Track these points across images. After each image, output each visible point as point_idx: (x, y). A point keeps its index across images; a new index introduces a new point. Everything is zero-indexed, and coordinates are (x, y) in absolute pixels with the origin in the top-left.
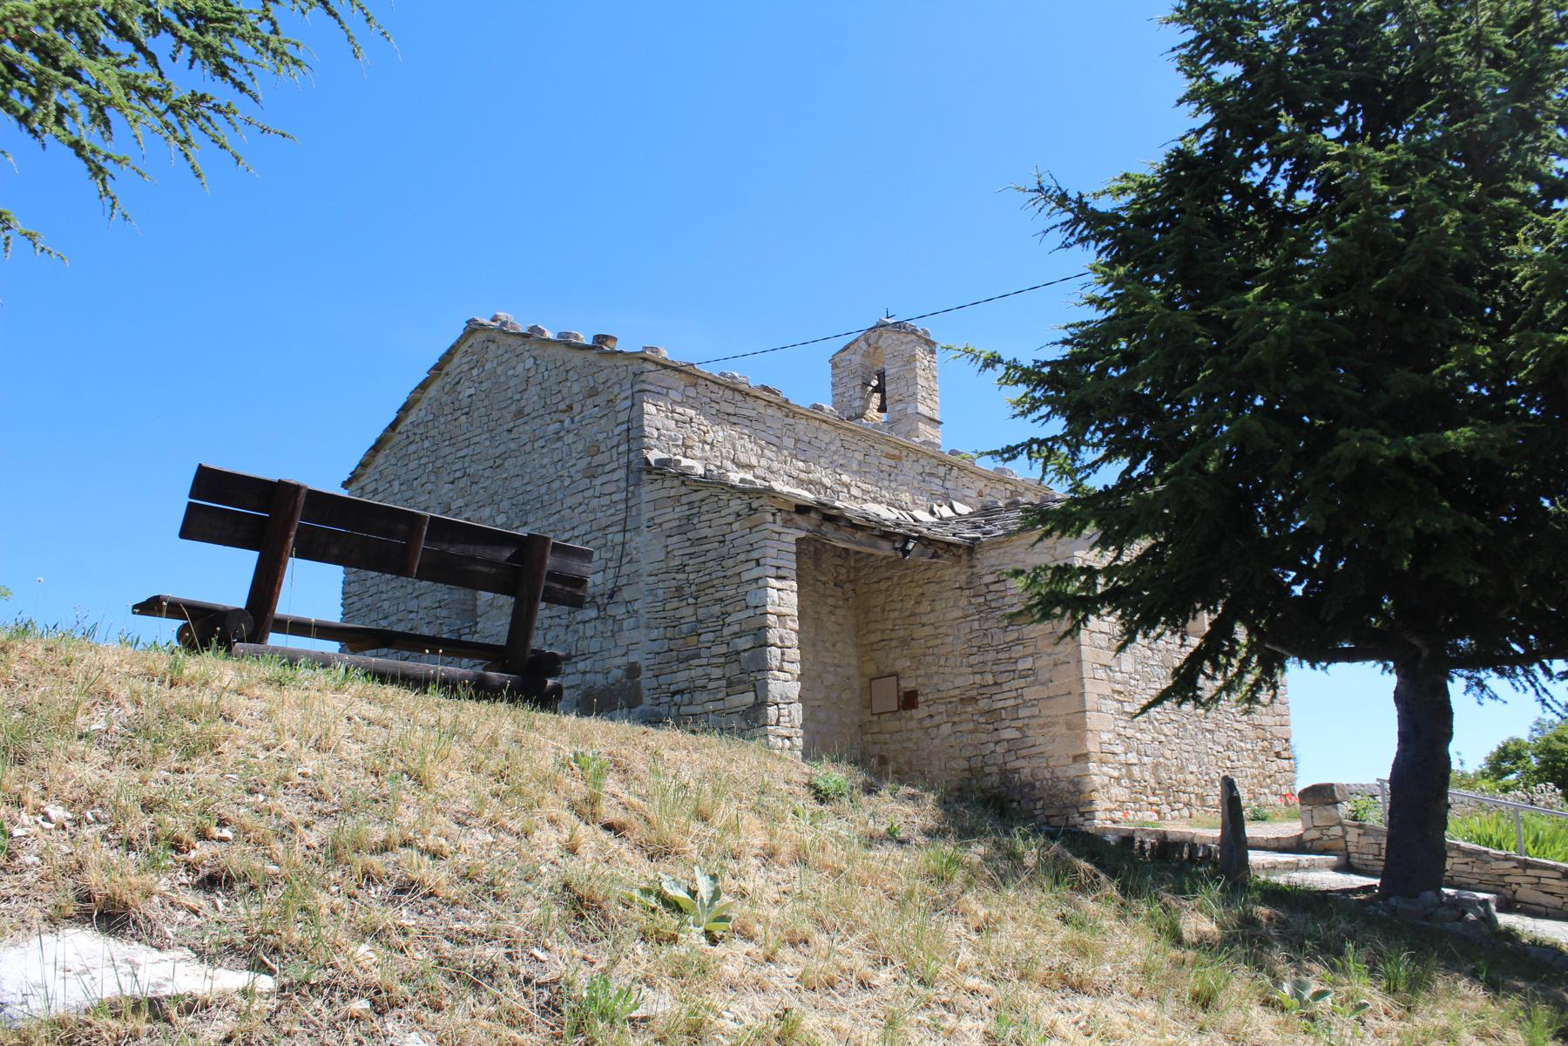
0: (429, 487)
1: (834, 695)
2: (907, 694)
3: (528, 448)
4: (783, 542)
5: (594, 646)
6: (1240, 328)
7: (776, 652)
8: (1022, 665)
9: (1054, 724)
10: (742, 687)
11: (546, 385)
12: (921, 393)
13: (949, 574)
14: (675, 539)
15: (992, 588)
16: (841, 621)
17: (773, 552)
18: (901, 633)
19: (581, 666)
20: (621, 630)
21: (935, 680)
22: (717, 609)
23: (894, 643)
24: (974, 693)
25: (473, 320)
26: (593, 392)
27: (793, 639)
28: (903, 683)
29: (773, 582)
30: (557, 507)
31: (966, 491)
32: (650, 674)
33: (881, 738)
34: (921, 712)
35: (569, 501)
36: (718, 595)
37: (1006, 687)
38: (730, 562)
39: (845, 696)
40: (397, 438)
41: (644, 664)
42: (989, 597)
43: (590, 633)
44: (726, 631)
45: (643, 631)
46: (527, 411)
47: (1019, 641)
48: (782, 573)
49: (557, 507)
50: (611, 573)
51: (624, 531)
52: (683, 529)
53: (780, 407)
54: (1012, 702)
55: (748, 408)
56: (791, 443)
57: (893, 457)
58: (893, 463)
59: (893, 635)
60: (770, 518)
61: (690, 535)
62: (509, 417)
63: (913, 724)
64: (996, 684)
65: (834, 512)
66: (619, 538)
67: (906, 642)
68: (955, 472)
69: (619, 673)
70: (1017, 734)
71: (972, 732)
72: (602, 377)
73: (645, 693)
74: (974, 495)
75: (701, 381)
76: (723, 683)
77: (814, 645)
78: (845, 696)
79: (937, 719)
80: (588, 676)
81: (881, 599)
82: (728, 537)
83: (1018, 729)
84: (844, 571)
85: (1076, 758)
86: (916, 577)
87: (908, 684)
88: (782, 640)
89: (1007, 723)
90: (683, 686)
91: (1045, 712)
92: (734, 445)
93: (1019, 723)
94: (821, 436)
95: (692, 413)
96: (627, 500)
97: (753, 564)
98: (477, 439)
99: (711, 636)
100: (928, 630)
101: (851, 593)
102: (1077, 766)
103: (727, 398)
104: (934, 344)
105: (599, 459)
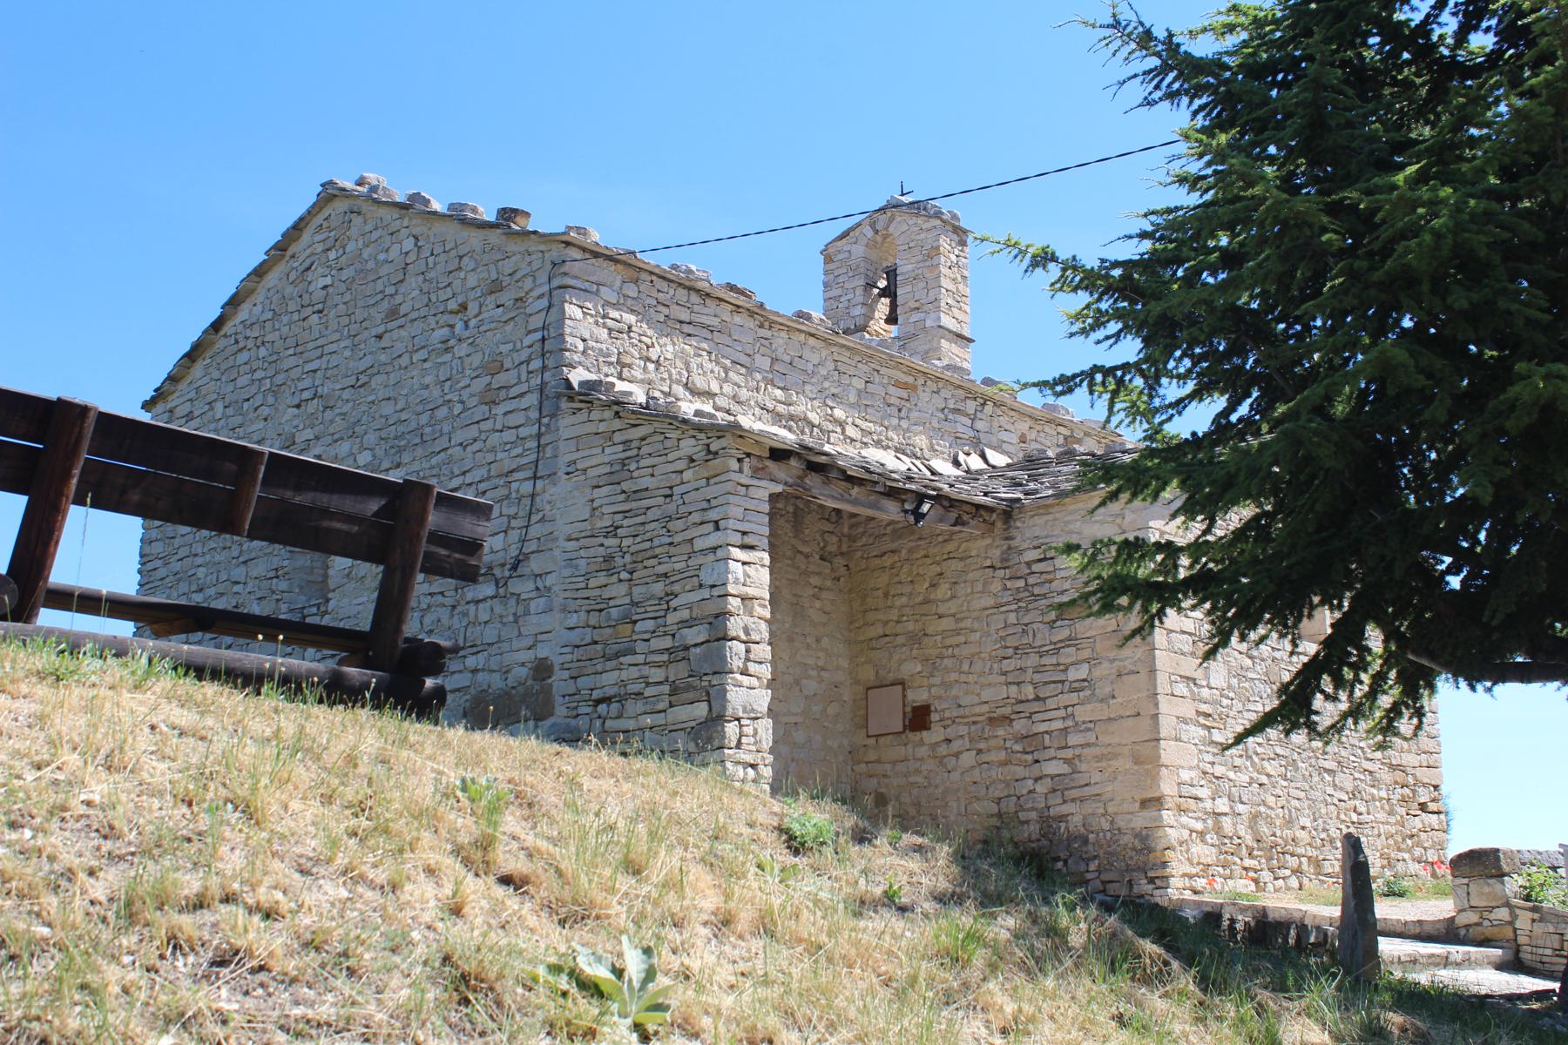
0: (265, 411)
1: (815, 709)
3: (405, 360)
5: (490, 634)
8: (1073, 675)
9: (1115, 756)
10: (691, 695)
14: (605, 491)
15: (1035, 568)
16: (828, 608)
17: (739, 512)
18: (911, 626)
20: (527, 613)
21: (954, 692)
22: (658, 589)
23: (900, 640)
24: (1007, 710)
26: (496, 287)
27: (763, 631)
28: (911, 695)
29: (736, 553)
31: (1004, 436)
34: (934, 735)
35: (459, 437)
36: (661, 569)
37: (1051, 704)
40: (221, 343)
41: (557, 660)
42: (1031, 580)
43: (484, 617)
44: (672, 618)
45: (558, 615)
47: (1071, 641)
50: (514, 535)
51: (535, 478)
52: (615, 478)
53: (752, 314)
54: (1059, 725)
55: (708, 314)
56: (765, 363)
57: (905, 386)
58: (904, 394)
59: (899, 628)
60: (735, 465)
61: (625, 486)
63: (923, 751)
66: (527, 488)
67: (916, 639)
68: (989, 408)
69: (523, 672)
70: (1065, 769)
73: (558, 700)
74: (1015, 440)
75: (644, 276)
76: (666, 689)
77: (791, 640)
80: (480, 676)
81: (883, 579)
83: (1066, 761)
84: (834, 539)
85: (1145, 803)
87: (918, 697)
88: (746, 630)
89: (1052, 753)
91: (1104, 739)
92: (687, 364)
93: (1069, 754)
95: (630, 318)
96: (539, 435)
97: (711, 527)
99: (650, 625)
100: (946, 624)
101: (843, 569)
102: (1145, 813)
105: (502, 379)
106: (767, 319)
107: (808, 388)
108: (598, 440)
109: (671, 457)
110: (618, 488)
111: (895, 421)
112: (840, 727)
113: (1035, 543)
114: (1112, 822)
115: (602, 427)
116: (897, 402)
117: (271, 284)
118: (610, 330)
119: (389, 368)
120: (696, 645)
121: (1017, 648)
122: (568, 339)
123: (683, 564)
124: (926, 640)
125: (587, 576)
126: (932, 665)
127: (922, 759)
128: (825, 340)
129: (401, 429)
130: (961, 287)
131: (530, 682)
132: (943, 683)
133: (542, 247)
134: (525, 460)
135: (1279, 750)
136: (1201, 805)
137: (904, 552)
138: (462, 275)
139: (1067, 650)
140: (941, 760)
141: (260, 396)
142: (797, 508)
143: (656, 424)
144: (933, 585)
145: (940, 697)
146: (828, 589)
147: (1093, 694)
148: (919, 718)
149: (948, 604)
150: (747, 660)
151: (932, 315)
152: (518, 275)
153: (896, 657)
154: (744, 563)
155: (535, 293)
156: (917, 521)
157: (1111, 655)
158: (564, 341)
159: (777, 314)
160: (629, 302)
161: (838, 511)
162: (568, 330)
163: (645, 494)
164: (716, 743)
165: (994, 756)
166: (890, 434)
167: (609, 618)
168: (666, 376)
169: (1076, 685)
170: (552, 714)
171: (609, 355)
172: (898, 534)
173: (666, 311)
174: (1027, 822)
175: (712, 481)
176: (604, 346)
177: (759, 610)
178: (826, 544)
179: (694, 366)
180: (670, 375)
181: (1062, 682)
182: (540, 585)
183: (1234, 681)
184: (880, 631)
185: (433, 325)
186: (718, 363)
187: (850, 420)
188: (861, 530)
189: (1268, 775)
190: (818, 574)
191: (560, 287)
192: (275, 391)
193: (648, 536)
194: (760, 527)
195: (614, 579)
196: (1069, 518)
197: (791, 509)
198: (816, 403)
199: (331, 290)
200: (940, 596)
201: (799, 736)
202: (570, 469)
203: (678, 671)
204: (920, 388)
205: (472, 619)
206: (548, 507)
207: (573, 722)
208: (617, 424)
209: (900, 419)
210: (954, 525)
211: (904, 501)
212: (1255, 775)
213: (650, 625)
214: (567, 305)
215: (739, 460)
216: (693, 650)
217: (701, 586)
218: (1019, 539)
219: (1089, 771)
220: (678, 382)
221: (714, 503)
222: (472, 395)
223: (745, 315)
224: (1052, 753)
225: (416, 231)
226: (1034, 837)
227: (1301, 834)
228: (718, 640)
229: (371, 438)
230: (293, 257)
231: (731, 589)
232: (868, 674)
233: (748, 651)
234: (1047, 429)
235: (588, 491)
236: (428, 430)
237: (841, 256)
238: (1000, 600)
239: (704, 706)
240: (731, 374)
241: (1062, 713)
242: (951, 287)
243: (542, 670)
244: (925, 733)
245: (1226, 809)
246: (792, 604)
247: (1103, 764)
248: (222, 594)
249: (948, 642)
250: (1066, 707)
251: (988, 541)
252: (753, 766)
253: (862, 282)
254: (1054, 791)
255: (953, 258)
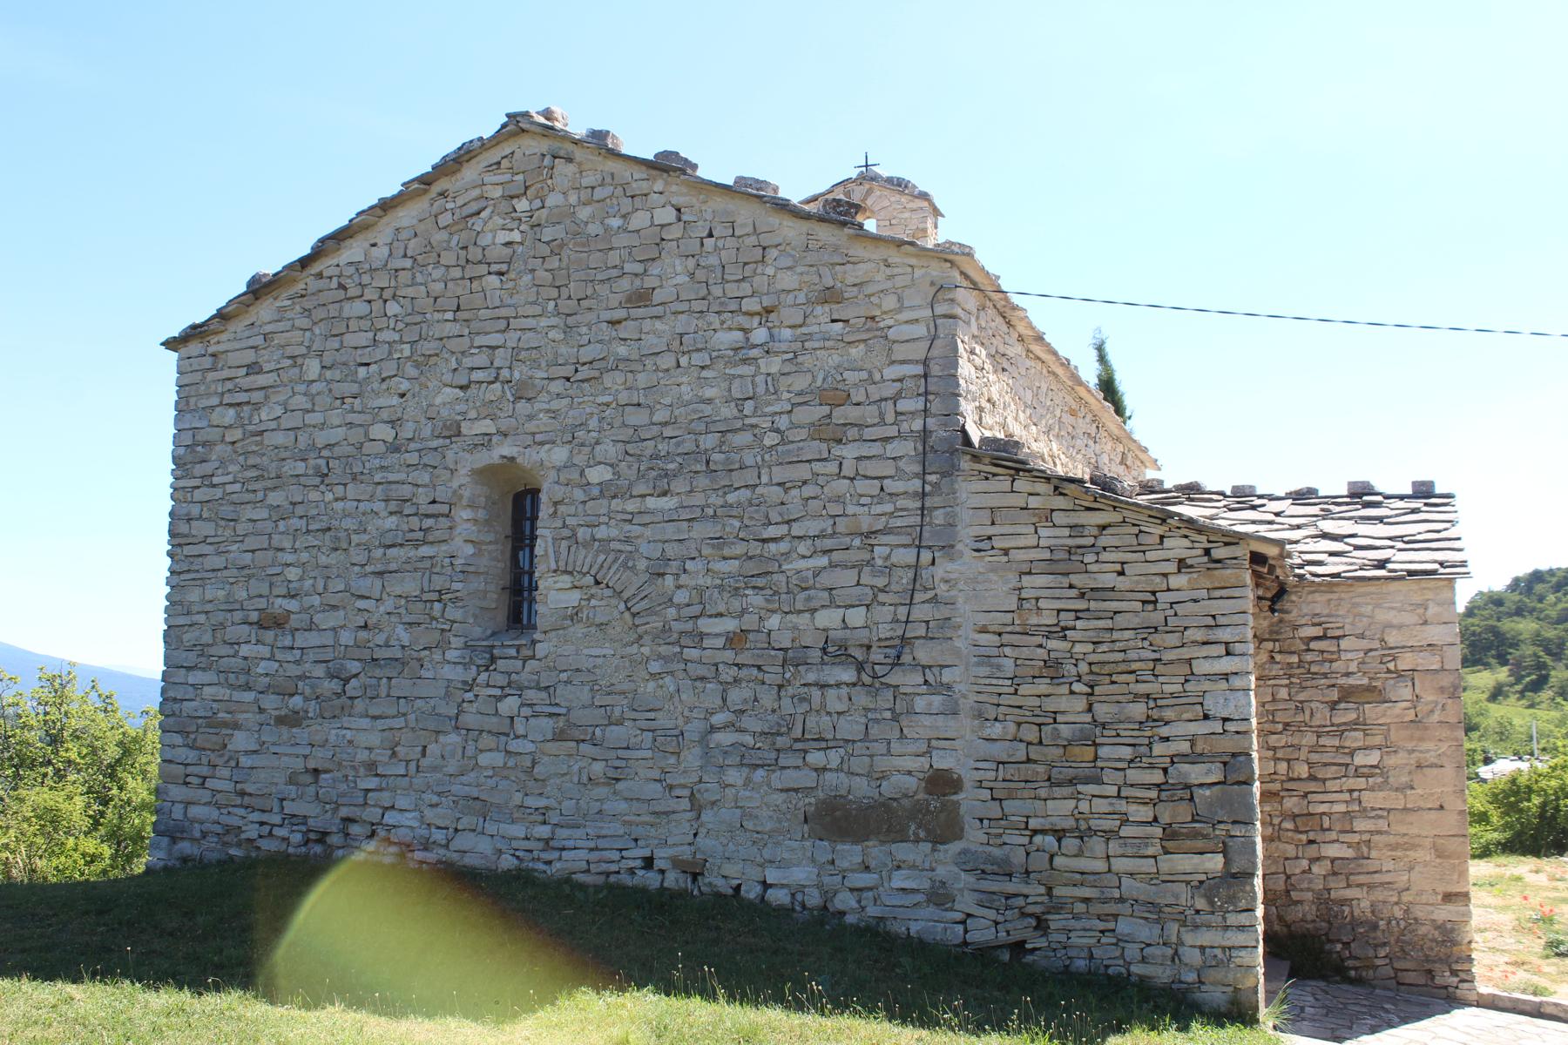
8: (1360, 759)
9: (1414, 847)
10: (1200, 844)
15: (1313, 645)
36: (1142, 688)
41: (969, 777)
46: (658, 297)
47: (1355, 725)
54: (1342, 808)
61: (1074, 579)
64: (1312, 778)
66: (908, 556)
69: (911, 783)
85: (1448, 897)
89: (1334, 835)
91: (1396, 828)
93: (1356, 838)
97: (1222, 650)
102: (1450, 907)
110: (1065, 581)
113: (1316, 620)
117: (405, 222)
123: (1178, 688)
129: (663, 447)
131: (921, 796)
133: (913, 261)
139: (1353, 734)
143: (1126, 513)
147: (1386, 782)
152: (869, 289)
164: (1243, 904)
169: (1365, 770)
182: (931, 679)
192: (423, 363)
193: (1118, 646)
195: (1065, 689)
196: (1357, 600)
206: (944, 587)
207: (997, 852)
208: (1060, 502)
218: (1294, 613)
219: (1381, 858)
221: (1221, 620)
224: (1334, 835)
226: (1309, 918)
230: (443, 194)
236: (716, 457)
239: (1220, 858)
248: (334, 607)
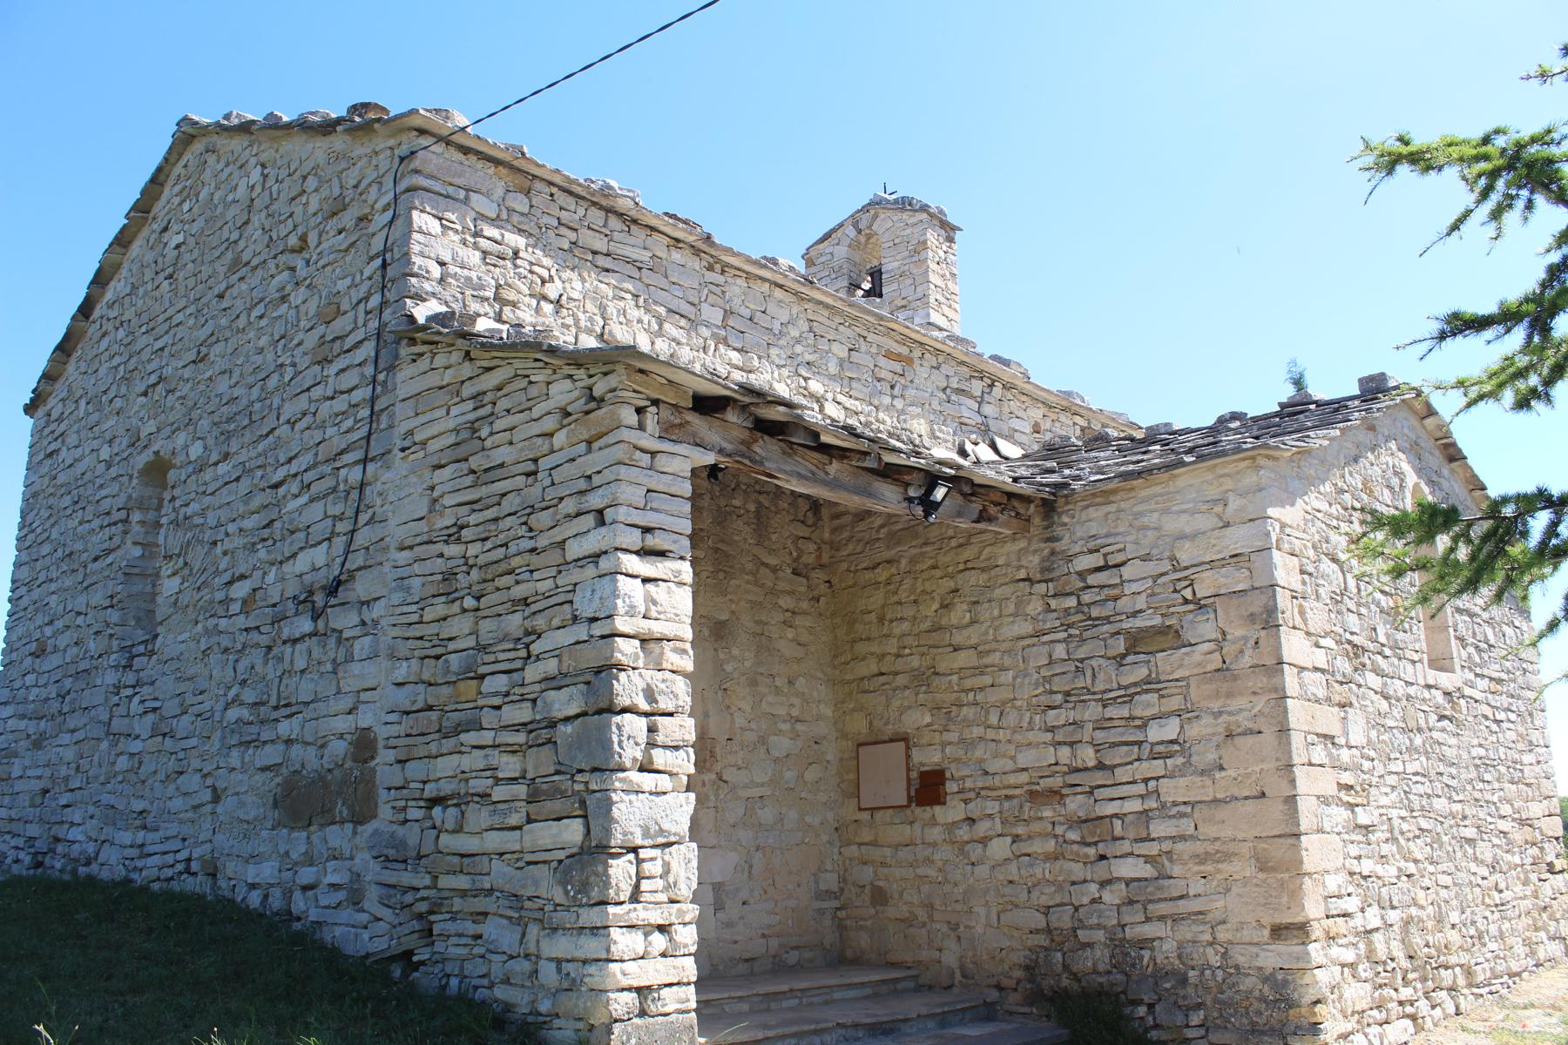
0: (118, 403)
1: (789, 775)
2: (924, 776)
3: (242, 322)
4: (660, 476)
5: (305, 689)
6: (422, 963)
7: (635, 725)
8: (1155, 733)
9: (1227, 857)
10: (556, 806)
11: (275, 207)
12: (934, 295)
13: (1006, 552)
14: (446, 473)
16: (804, 638)
17: (637, 496)
18: (915, 662)
19: (284, 728)
20: (349, 659)
21: (978, 753)
22: (514, 623)
23: (901, 680)
24: (1056, 782)
25: (186, 119)
26: (338, 207)
27: (679, 693)
28: (917, 756)
29: (631, 562)
30: (270, 422)
31: (1015, 424)
32: (390, 756)
33: (876, 853)
34: (952, 811)
35: (289, 411)
36: (519, 592)
37: (1122, 774)
38: (542, 519)
39: (810, 776)
40: (93, 330)
41: (382, 732)
42: (1087, 597)
43: (300, 664)
44: (532, 673)
45: (384, 663)
46: (245, 257)
47: (1150, 684)
48: (653, 541)
49: (270, 422)
50: (339, 543)
51: (365, 461)
52: (461, 451)
53: (697, 252)
54: (1134, 806)
55: (633, 246)
56: (716, 316)
57: (898, 358)
58: (898, 367)
59: (900, 665)
60: (633, 419)
61: (474, 463)
62: (222, 270)
63: (935, 834)
64: (1101, 766)
65: (778, 414)
66: (355, 475)
67: (924, 678)
68: (998, 390)
69: (339, 748)
70: (1147, 871)
71: (1055, 857)
72: (351, 178)
73: (383, 793)
74: (1028, 430)
75: (538, 185)
76: (521, 790)
77: (753, 683)
78: (810, 776)
79: (982, 828)
80: (296, 750)
81: (878, 598)
82: (544, 464)
83: (1148, 859)
84: (812, 547)
85: (1279, 932)
86: (943, 559)
87: (928, 758)
88: (650, 694)
89: (1126, 846)
90: (447, 788)
91: (1207, 830)
92: (603, 309)
93: (1152, 849)
94: (772, 308)
95: (520, 241)
96: (373, 400)
97: (589, 520)
98: (179, 317)
99: (501, 682)
100: (965, 659)
101: (823, 588)
102: (1280, 947)
103: (593, 222)
104: (954, 229)
105: (342, 325)
106: (718, 261)
107: (774, 351)
108: (442, 397)
109: (536, 413)
110: (464, 465)
111: (887, 400)
112: (822, 797)
113: (1091, 545)
114: (1225, 955)
115: (448, 377)
116: (890, 376)
118: (485, 253)
119: (228, 334)
120: (567, 719)
121: (1067, 694)
122: (417, 260)
123: (549, 584)
124: (937, 681)
125: (422, 603)
126: (945, 714)
127: (934, 845)
128: (796, 294)
130: (950, 284)
132: (962, 741)
133: (392, 142)
134: (356, 436)
135: (1424, 824)
136: (1351, 923)
137: (904, 562)
138: (304, 200)
139: (1144, 697)
140: (962, 847)
141: (114, 387)
142: (760, 505)
143: (518, 364)
144: (945, 606)
145: (957, 760)
146: (805, 613)
148: (929, 788)
149: (966, 632)
150: (651, 744)
151: (921, 312)
153: (896, 703)
154: (646, 580)
155: (379, 206)
156: (927, 514)
157: (1216, 706)
158: (409, 263)
159: (729, 251)
160: (516, 218)
161: (815, 505)
162: (416, 248)
163: (499, 473)
164: (595, 894)
165: (1037, 847)
166: (881, 415)
167: (447, 671)
168: (569, 321)
169: (1161, 748)
170: (375, 816)
171: (482, 288)
172: (910, 531)
173: (572, 236)
174: (1090, 945)
175: (596, 445)
176: (474, 275)
177: (672, 658)
178: (801, 553)
179: (612, 310)
180: (577, 321)
181: (1139, 743)
183: (1373, 734)
184: (874, 668)
185: (273, 271)
186: (648, 311)
187: (830, 396)
188: (846, 535)
189: (1416, 861)
190: (791, 593)
191: (408, 190)
193: (502, 538)
194: (678, 521)
195: (456, 608)
197: (752, 507)
198: (785, 371)
199: (183, 248)
200: (954, 621)
201: (766, 815)
202: (407, 443)
203: (540, 762)
204: (917, 362)
205: (286, 665)
207: (400, 831)
208: (467, 370)
209: (893, 397)
210: (977, 521)
211: (907, 485)
212: (1402, 864)
213: (501, 682)
214: (415, 214)
215: (640, 411)
216: (561, 727)
217: (575, 618)
218: (1066, 540)
219: (1186, 876)
220: (589, 331)
222: (305, 354)
223: (688, 251)
224: (1126, 846)
225: (264, 157)
227: (1453, 936)
228: (600, 712)
229: (205, 423)
231: (621, 624)
232: (858, 725)
233: (652, 730)
234: (1063, 418)
235: (427, 473)
237: (823, 259)
238: (1041, 626)
240: (667, 326)
241: (1140, 789)
242: (940, 282)
243: (364, 744)
244: (938, 809)
245: (1376, 923)
246: (755, 634)
247: (1208, 868)
249: (968, 683)
250: (1146, 781)
251: (1022, 544)
252: (662, 929)
253: (846, 283)
254: (1131, 902)
255: (941, 253)
